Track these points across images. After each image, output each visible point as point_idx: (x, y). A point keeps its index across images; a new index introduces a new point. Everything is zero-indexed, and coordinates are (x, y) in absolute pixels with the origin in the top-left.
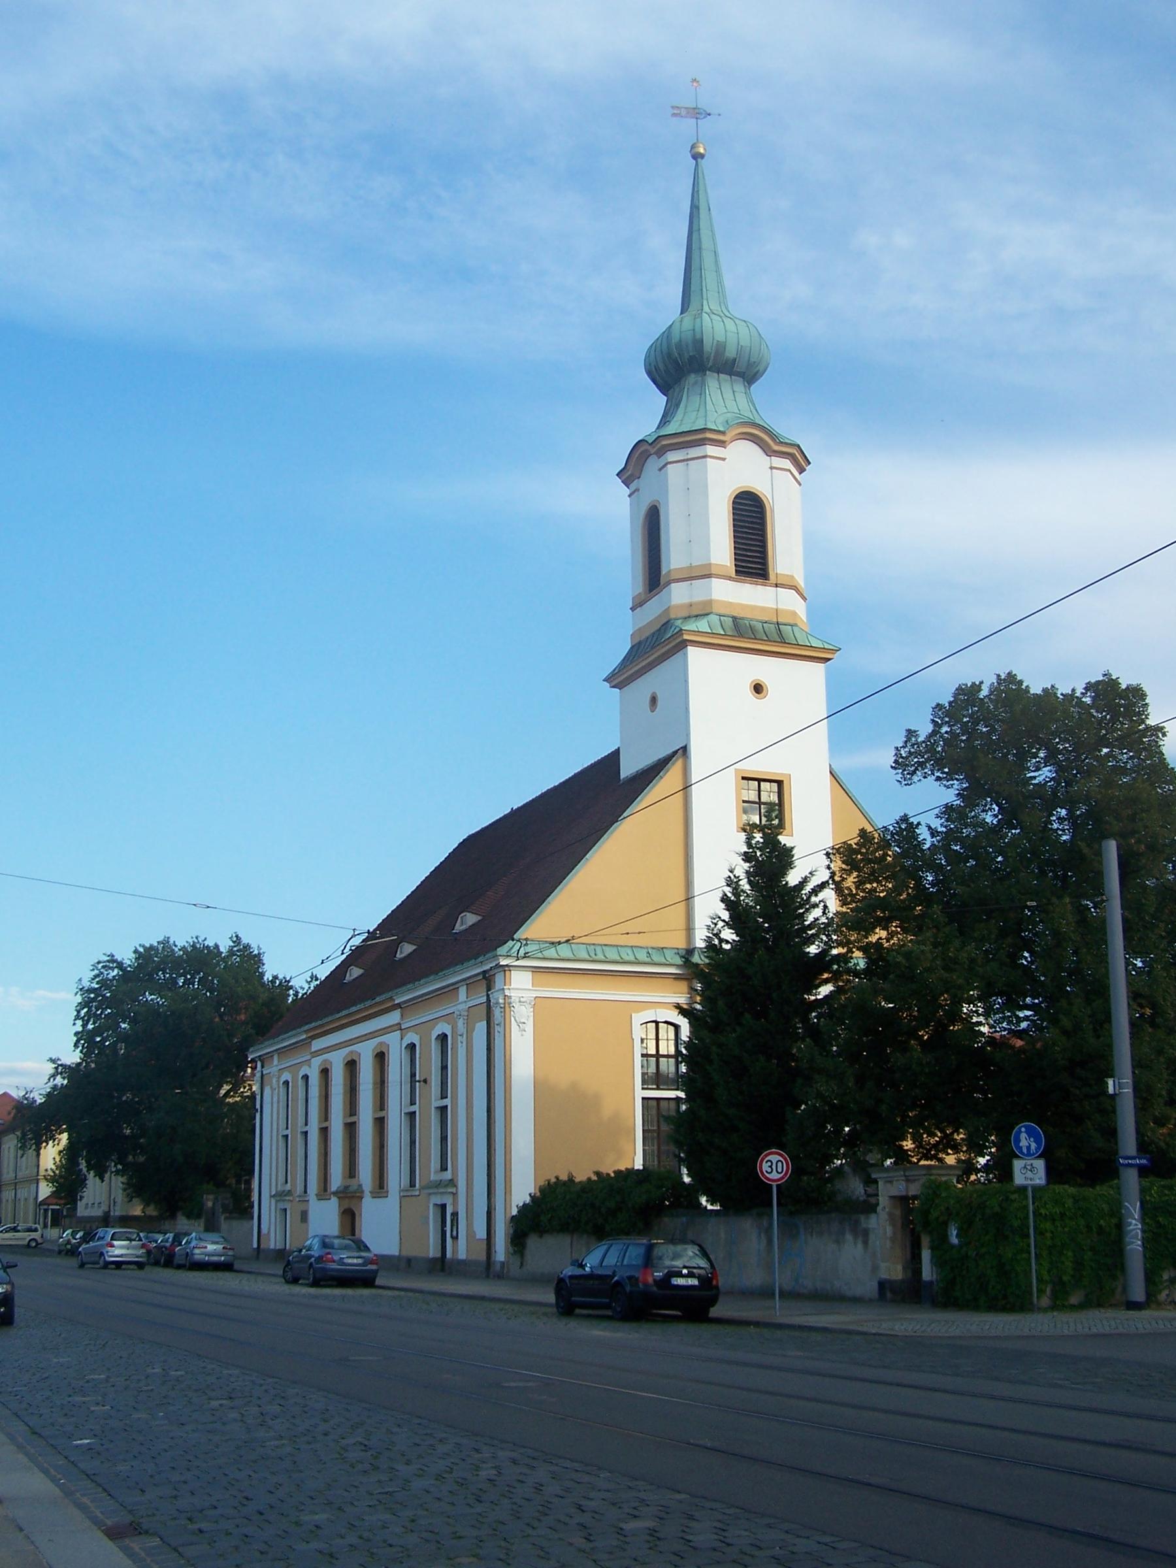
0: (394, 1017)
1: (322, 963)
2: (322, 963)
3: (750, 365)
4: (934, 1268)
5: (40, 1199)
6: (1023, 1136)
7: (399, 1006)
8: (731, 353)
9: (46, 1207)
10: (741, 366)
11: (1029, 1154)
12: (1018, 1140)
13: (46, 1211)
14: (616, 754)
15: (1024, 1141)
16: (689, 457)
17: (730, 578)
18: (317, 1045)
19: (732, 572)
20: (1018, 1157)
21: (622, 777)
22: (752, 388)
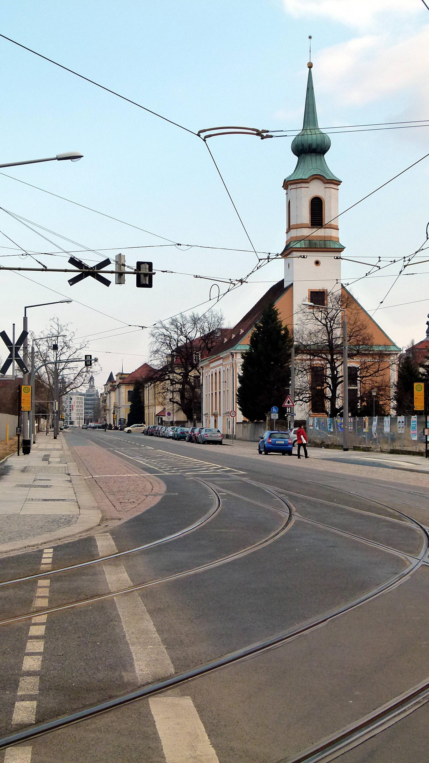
0: (221, 361)
1: (366, 275)
2: (366, 275)
3: (321, 149)
4: (142, 400)
5: (156, 414)
6: (274, 409)
7: (222, 358)
8: (314, 146)
9: (158, 417)
10: (319, 150)
11: (275, 413)
12: (273, 410)
13: (158, 418)
14: (283, 281)
15: (274, 410)
16: (297, 187)
17: (309, 228)
18: (212, 365)
19: (310, 226)
20: (272, 413)
21: (285, 287)
22: (325, 155)
